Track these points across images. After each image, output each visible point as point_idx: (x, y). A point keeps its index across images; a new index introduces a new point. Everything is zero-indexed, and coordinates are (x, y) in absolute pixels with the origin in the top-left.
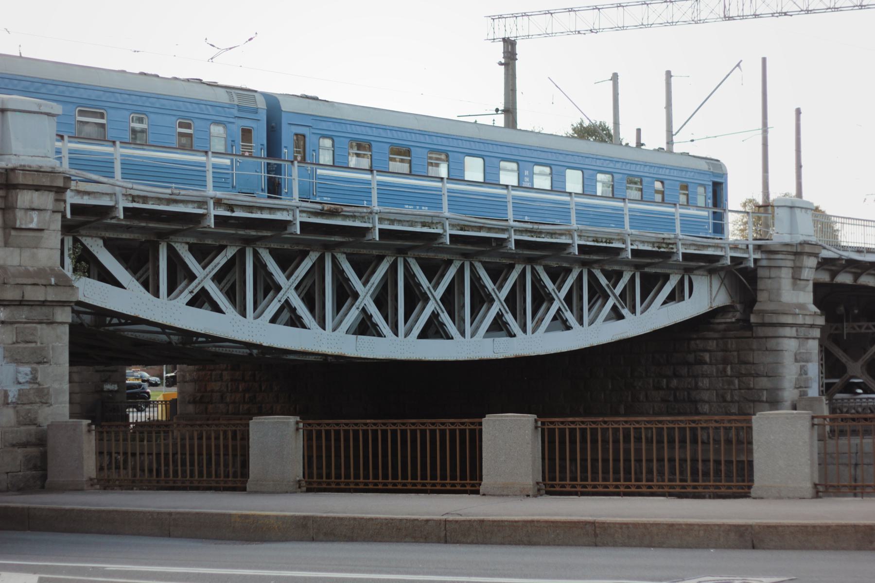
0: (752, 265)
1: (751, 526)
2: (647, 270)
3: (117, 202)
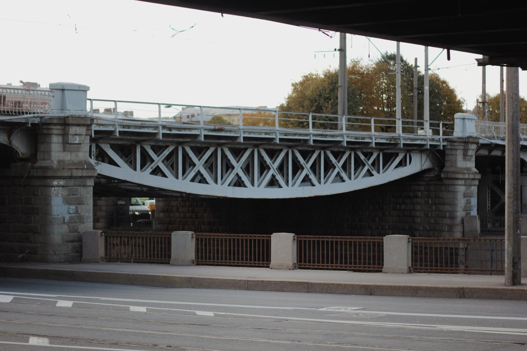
0: (442, 148)
1: (370, 286)
2: (386, 151)
3: (116, 129)
